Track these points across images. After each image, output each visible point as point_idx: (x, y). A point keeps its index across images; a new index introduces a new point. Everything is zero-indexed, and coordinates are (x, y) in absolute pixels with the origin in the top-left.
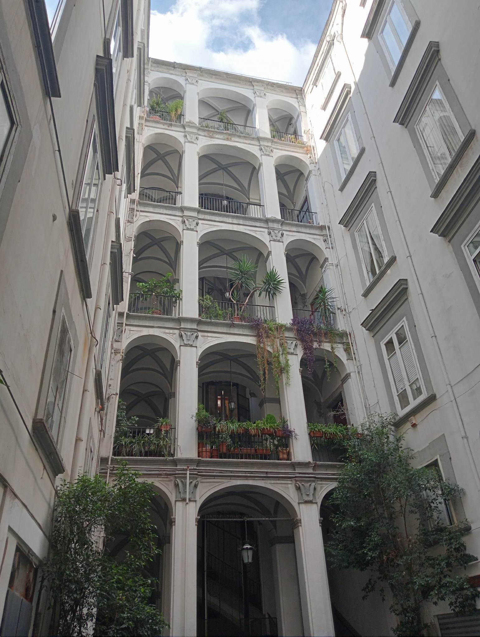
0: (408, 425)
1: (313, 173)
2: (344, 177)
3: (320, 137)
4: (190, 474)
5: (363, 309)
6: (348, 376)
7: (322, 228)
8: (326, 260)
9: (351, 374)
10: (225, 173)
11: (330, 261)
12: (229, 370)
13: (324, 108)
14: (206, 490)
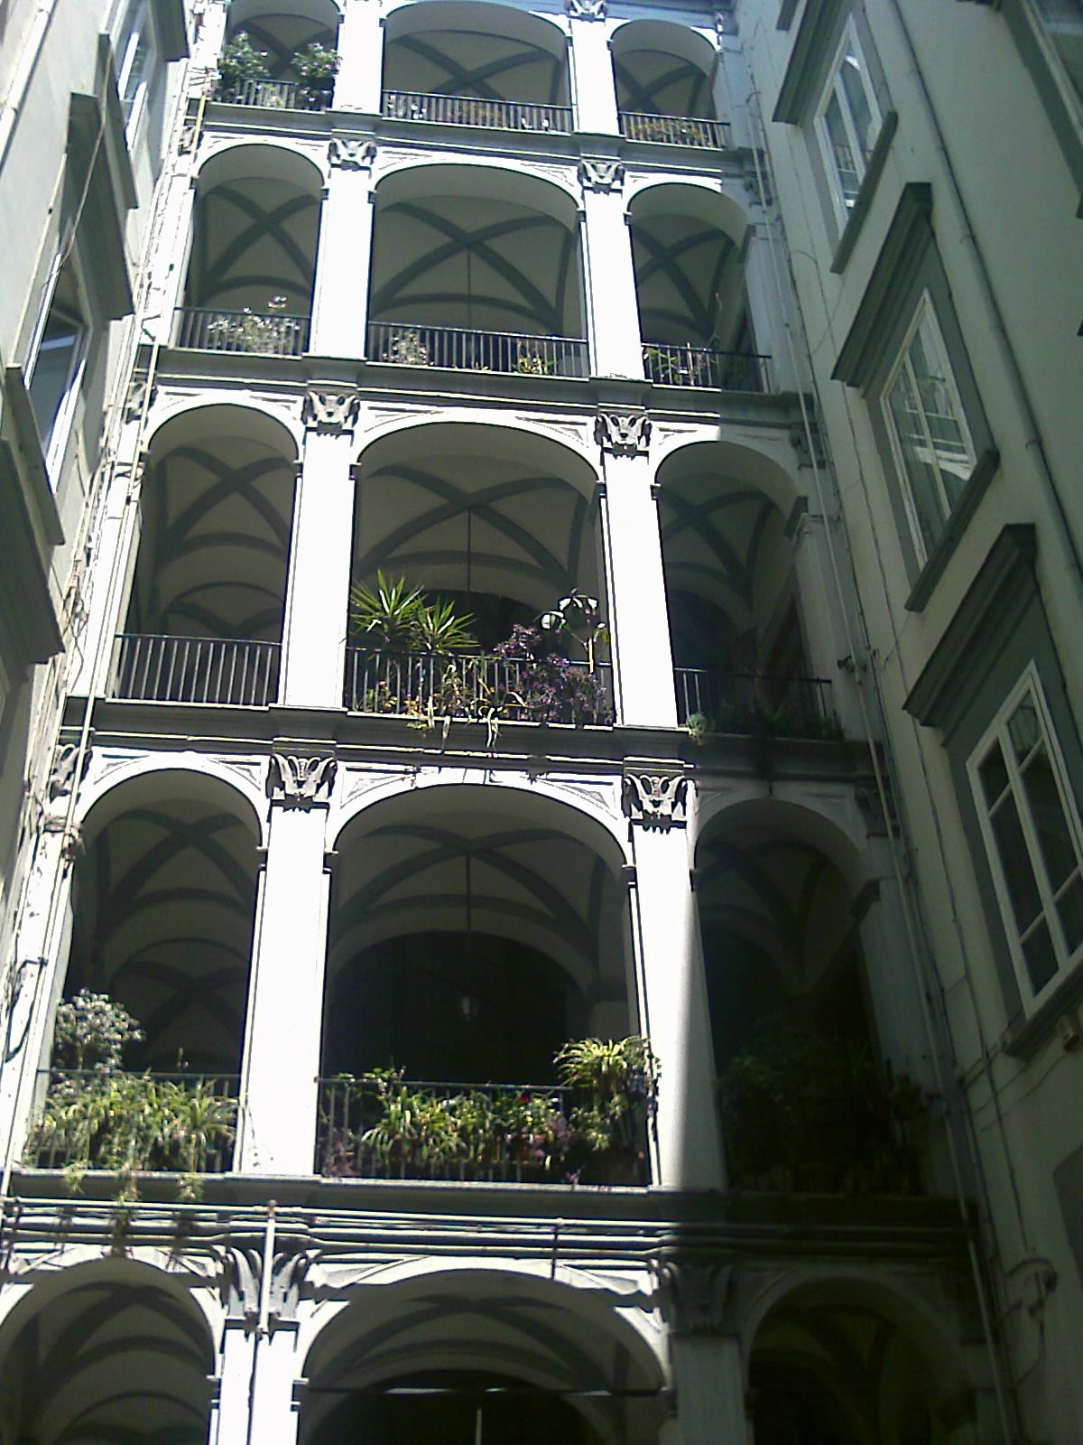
0: (1056, 1047)
1: (760, 231)
2: (842, 221)
3: (831, 371)
4: (277, 1230)
5: (908, 647)
6: (872, 890)
7: (786, 403)
8: (802, 503)
9: (883, 886)
10: (475, 260)
11: (813, 509)
12: (463, 290)
13: (784, 24)
14: (359, 788)
